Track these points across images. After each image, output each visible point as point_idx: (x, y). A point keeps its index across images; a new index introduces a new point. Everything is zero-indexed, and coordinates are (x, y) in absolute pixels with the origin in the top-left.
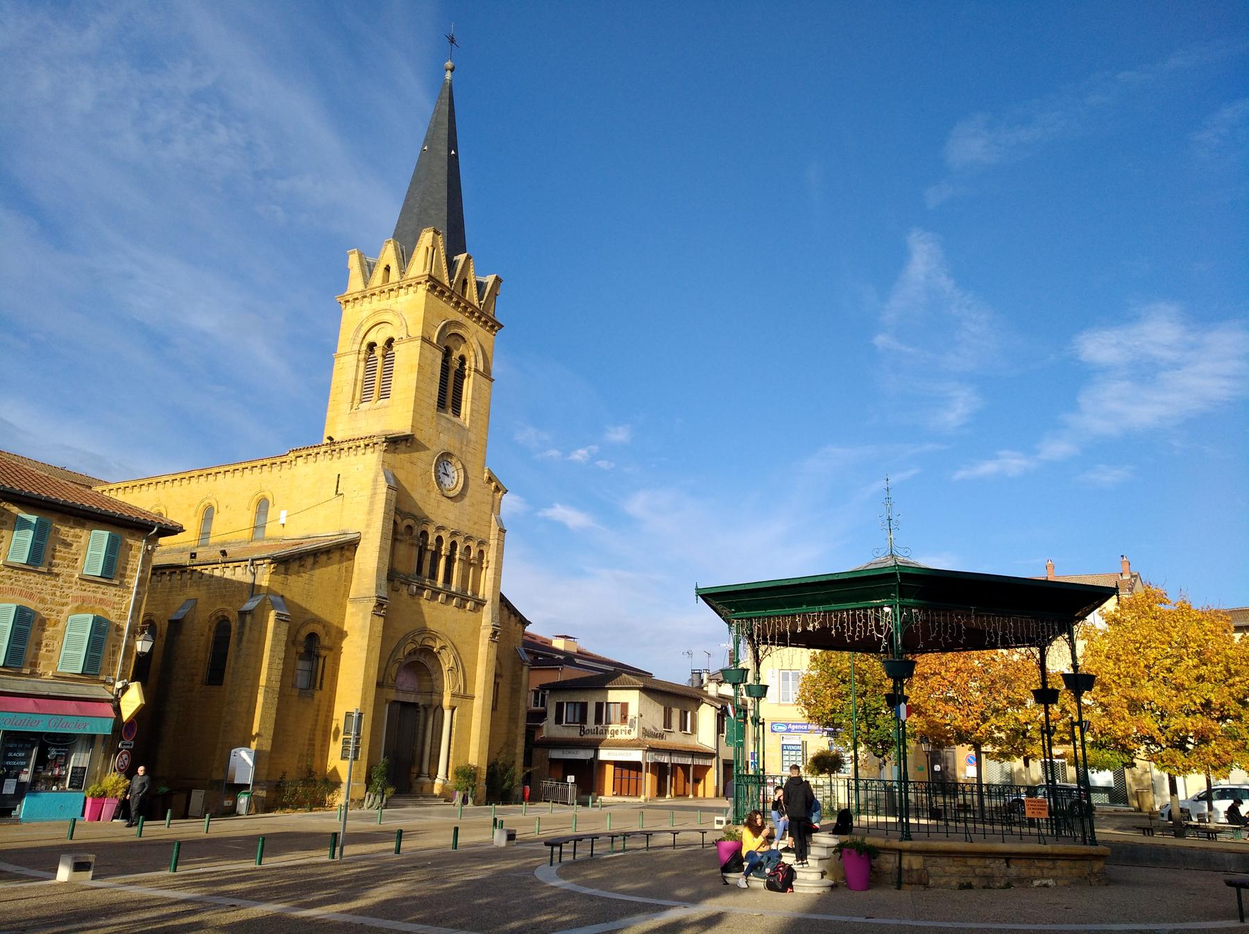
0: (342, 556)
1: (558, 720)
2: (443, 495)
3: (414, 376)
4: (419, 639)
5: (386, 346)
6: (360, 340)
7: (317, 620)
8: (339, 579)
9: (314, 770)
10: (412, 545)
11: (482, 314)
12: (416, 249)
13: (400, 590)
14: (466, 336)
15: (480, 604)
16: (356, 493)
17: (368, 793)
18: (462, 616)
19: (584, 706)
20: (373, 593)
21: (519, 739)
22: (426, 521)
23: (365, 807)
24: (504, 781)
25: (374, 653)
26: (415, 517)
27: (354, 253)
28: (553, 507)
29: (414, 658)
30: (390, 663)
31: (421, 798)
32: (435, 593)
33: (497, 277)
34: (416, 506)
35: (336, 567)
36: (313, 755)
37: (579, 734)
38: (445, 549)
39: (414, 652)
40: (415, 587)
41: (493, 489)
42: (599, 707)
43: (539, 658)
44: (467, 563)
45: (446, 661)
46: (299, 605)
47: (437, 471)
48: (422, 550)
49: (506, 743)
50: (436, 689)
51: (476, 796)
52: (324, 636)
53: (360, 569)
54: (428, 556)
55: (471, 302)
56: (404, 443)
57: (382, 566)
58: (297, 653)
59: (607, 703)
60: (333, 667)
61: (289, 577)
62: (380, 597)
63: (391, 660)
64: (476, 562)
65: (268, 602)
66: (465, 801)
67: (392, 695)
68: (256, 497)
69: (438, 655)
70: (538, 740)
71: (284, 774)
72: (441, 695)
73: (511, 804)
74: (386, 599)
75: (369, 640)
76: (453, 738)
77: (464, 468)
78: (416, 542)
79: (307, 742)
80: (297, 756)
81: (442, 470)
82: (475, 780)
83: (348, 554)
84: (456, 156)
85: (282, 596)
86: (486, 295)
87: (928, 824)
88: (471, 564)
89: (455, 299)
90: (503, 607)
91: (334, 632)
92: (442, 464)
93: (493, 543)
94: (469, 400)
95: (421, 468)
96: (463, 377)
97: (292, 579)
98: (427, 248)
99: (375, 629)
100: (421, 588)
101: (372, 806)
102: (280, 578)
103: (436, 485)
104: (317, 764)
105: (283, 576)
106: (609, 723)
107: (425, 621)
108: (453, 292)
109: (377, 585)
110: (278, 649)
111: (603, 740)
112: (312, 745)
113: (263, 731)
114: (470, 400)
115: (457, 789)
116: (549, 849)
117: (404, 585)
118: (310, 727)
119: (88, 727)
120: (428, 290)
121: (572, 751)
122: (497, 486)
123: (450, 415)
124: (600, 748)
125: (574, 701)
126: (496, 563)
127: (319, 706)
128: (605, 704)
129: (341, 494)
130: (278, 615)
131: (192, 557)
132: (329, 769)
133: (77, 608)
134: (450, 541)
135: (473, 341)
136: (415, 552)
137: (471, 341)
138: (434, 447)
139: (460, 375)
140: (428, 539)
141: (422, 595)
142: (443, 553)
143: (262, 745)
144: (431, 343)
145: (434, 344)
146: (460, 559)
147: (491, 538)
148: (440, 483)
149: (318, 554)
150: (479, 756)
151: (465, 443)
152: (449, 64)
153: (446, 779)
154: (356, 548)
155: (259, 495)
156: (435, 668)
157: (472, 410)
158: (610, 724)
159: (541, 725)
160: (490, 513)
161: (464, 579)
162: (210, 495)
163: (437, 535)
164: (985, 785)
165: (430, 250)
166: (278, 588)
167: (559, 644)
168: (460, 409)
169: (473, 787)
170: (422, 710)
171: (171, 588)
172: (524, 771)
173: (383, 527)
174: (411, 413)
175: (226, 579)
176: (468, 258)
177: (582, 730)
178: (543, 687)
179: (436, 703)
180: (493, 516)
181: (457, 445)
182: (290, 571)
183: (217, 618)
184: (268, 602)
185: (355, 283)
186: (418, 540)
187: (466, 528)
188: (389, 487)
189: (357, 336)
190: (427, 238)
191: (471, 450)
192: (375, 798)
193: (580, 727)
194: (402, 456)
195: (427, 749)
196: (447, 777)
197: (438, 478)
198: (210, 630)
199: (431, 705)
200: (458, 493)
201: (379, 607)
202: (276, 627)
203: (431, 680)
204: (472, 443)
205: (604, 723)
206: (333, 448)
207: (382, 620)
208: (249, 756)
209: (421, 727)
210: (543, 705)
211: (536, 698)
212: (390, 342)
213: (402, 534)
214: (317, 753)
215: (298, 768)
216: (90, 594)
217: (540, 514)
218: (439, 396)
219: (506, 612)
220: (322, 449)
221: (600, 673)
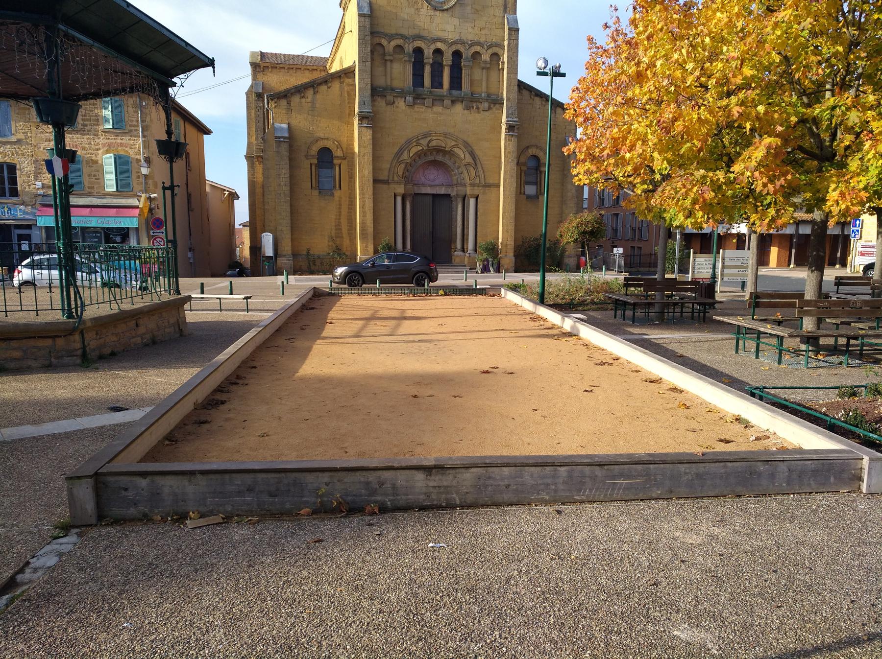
10: (405, 61)
13: (396, 103)
25: (366, 158)
36: (342, 237)
38: (447, 59)
71: (308, 250)
87: (175, 274)
116: (245, 300)
118: (334, 217)
119: (122, 223)
133: (107, 150)
136: (409, 69)
215: (329, 245)
216: (113, 141)
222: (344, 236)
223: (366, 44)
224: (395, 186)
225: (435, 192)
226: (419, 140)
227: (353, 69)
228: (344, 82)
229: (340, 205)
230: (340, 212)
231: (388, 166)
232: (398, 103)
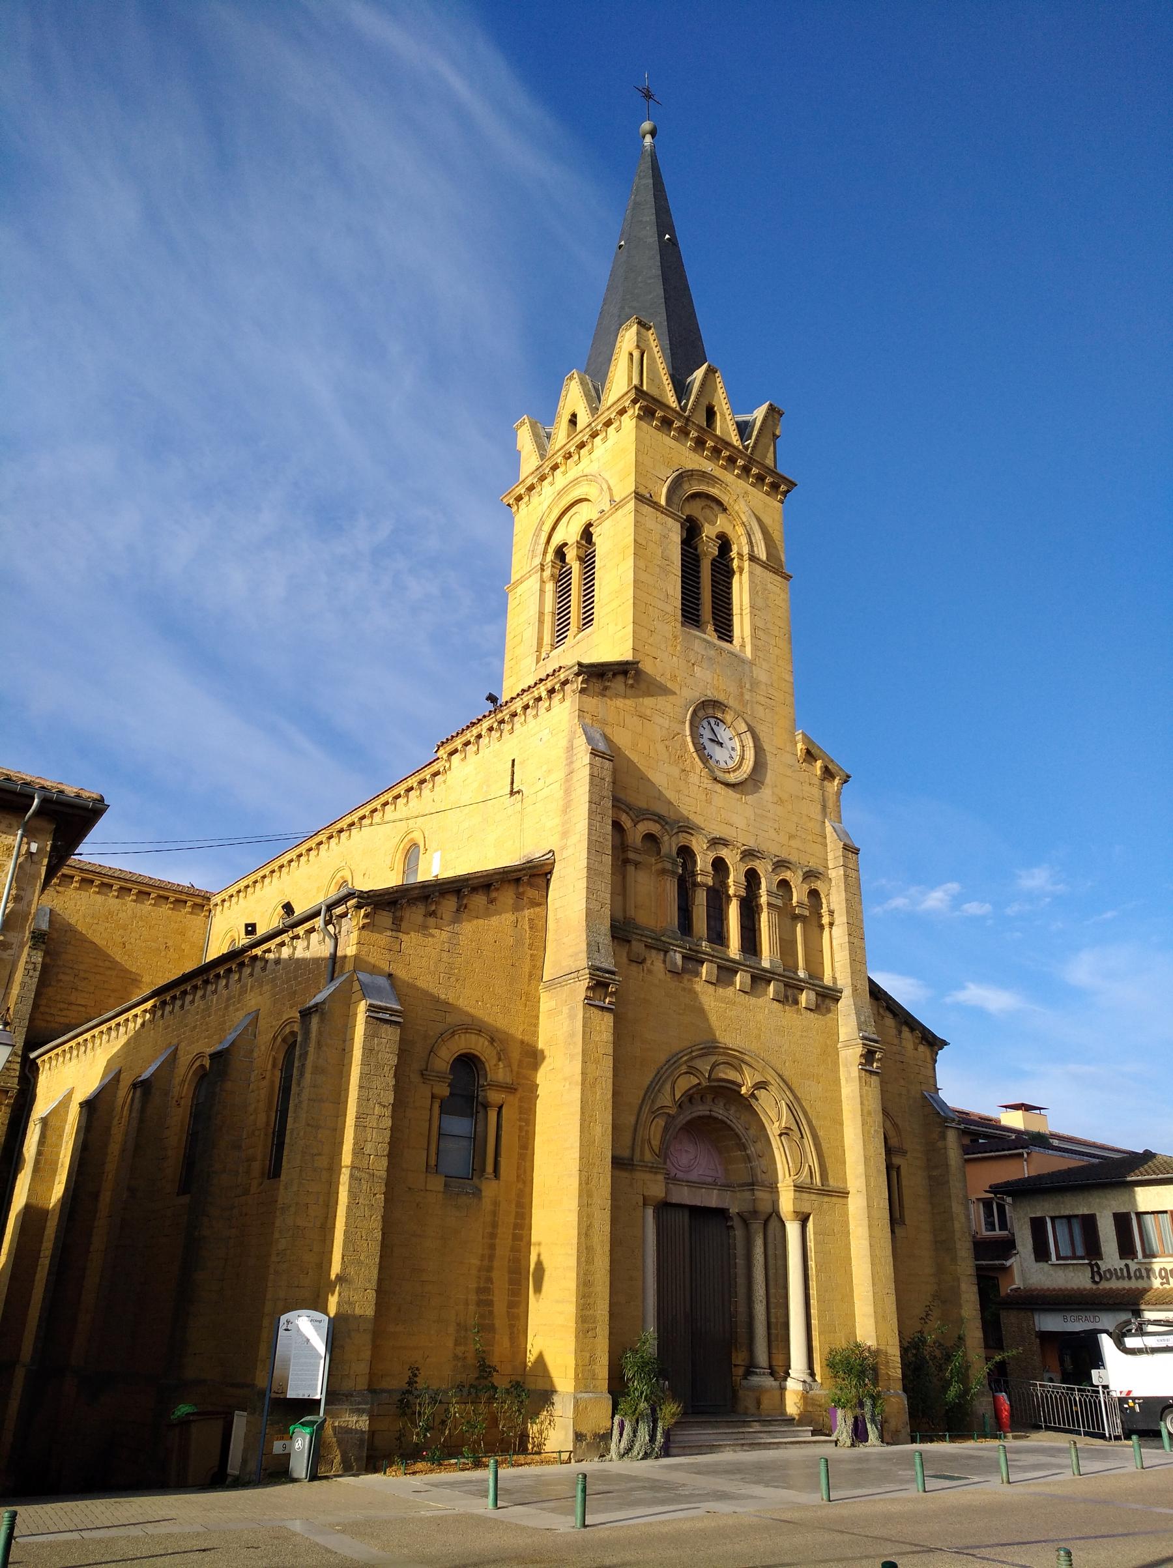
0: (519, 896)
1: (1041, 1253)
2: (715, 779)
3: (630, 562)
4: (704, 1066)
5: (583, 542)
6: (541, 547)
7: (474, 1027)
8: (519, 942)
9: (495, 1361)
10: (663, 872)
11: (751, 460)
12: (613, 363)
13: (649, 962)
14: (725, 499)
15: (828, 997)
16: (542, 781)
17: (617, 1418)
18: (788, 1017)
19: (1089, 1224)
20: (582, 962)
21: (964, 1286)
22: (687, 827)
23: (613, 1453)
24: (946, 1385)
26: (659, 819)
27: (523, 423)
28: (964, 988)
29: (701, 1110)
30: (643, 1117)
31: (757, 1427)
32: (727, 971)
33: (771, 405)
34: (660, 796)
35: (508, 918)
36: (491, 1328)
37: (1089, 1281)
38: (735, 883)
39: (691, 1097)
40: (678, 957)
41: (819, 773)
42: (1122, 1222)
43: (981, 1141)
44: (787, 915)
45: (773, 1114)
46: (431, 995)
47: (696, 736)
48: (686, 885)
49: (936, 1296)
50: (760, 1177)
51: (884, 1422)
52: (493, 1062)
53: (557, 920)
54: (701, 897)
55: (728, 439)
56: (620, 678)
57: (596, 906)
58: (433, 1097)
59: (1139, 1215)
60: (521, 1129)
61: (404, 937)
62: (599, 969)
63: (646, 1109)
64: (807, 913)
65: (356, 986)
66: (859, 1434)
67: (656, 1188)
68: (401, 847)
69: (753, 1101)
70: (1008, 1295)
71: (414, 1372)
72: (773, 1189)
73: (970, 1437)
74: (613, 973)
75: (584, 1062)
76: (813, 1284)
77: (751, 729)
78: (669, 866)
79: (473, 1297)
80: (452, 1329)
81: (707, 734)
82: (875, 1381)
83: (531, 893)
84: (673, 241)
85: (390, 975)
86: (755, 433)
88: (796, 918)
89: (693, 434)
90: (881, 1011)
91: (515, 1054)
92: (705, 723)
93: (836, 874)
94: (747, 611)
95: (661, 727)
96: (730, 573)
97: (410, 940)
98: (631, 354)
99: (596, 1038)
100: (694, 959)
101: (629, 1450)
102: (383, 938)
103: (697, 759)
104: (502, 1345)
105: (389, 933)
106: (1150, 1254)
107: (710, 1029)
108: (688, 419)
109: (588, 945)
110: (377, 1083)
111: (1145, 1291)
112: (485, 1304)
113: (352, 1271)
114: (748, 610)
115: (838, 1403)
117: (654, 952)
118: (476, 1262)
120: (639, 417)
121: (1083, 1315)
122: (826, 767)
123: (710, 635)
124: (1143, 1307)
125: (1067, 1213)
126: (848, 912)
127: (494, 1213)
128: (1133, 1217)
129: (518, 792)
130: (371, 1008)
131: (248, 933)
132: (531, 1358)
134: (743, 868)
135: (740, 508)
136: (671, 888)
137: (737, 508)
138: (684, 689)
139: (723, 571)
140: (695, 862)
141: (697, 974)
142: (731, 892)
143: (350, 1303)
144: (655, 505)
145: (660, 506)
146: (769, 904)
147: (830, 866)
148: (705, 758)
149: (466, 891)
150: (876, 1323)
151: (748, 686)
152: (647, 126)
153: (809, 1379)
154: (548, 881)
155: (406, 840)
156: (752, 1132)
157: (754, 628)
158: (1154, 1256)
160: (819, 818)
161: (786, 947)
162: (343, 864)
163: (711, 856)
165: (636, 354)
166: (377, 958)
167: (1014, 1120)
168: (731, 631)
169: (874, 1398)
170: (737, 1223)
171: (228, 999)
172: (988, 1359)
173: (590, 829)
174: (630, 628)
175: (298, 959)
176: (711, 371)
177: (1096, 1272)
178: (995, 1189)
179: (765, 1207)
180: (827, 823)
181: (733, 689)
182: (404, 925)
183: (284, 1040)
184: (356, 986)
185: (529, 461)
186: (674, 863)
187: (773, 844)
188: (595, 753)
189: (536, 543)
190: (628, 338)
191: (763, 700)
192: (635, 1431)
193: (1090, 1264)
194: (620, 703)
195: (760, 1309)
196: (812, 1374)
197: (700, 749)
198: (274, 1066)
199: (755, 1213)
200: (745, 776)
201: (600, 992)
202: (369, 1036)
203: (748, 1159)
204: (763, 687)
205: (1140, 1254)
206: (499, 716)
207: (609, 1019)
208: (317, 1329)
209: (740, 1261)
210: (1004, 1226)
211: (989, 1214)
212: (587, 535)
213: (636, 851)
214: (500, 1322)
215: (456, 1357)
217: (949, 1000)
218: (682, 598)
219: (889, 1021)
220: (484, 725)
221: (1098, 1160)
222: (498, 1323)
223: (603, 815)
224: (647, 1176)
225: (697, 1202)
227: (547, 869)
228: (523, 894)
229: (494, 1225)
230: (492, 1247)
231: (632, 1120)
232: (652, 964)
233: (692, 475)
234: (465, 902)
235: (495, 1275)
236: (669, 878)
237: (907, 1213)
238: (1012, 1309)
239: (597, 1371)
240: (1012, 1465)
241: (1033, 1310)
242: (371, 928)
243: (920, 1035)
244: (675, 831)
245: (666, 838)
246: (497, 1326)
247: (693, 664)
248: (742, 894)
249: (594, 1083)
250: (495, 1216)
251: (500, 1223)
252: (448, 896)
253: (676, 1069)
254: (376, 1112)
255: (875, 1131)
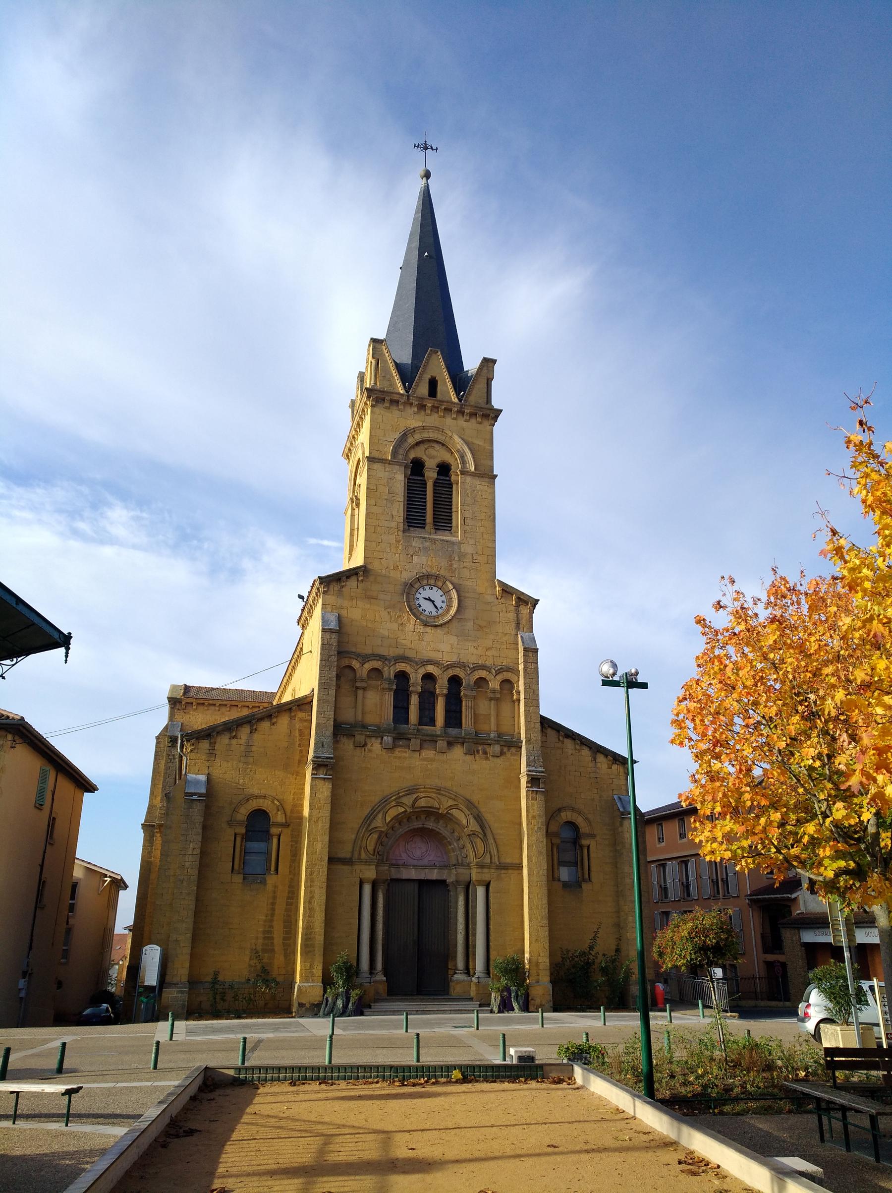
13: (369, 745)
56: (354, 578)
71: (216, 974)
78: (386, 686)
79: (261, 935)
127: (274, 892)
151: (456, 558)
159: (793, 896)
160: (514, 632)
164: (649, 981)
181: (444, 563)
195: (460, 938)
215: (250, 966)
224: (363, 867)
225: (422, 877)
226: (400, 797)
227: (309, 700)
228: (295, 716)
229: (275, 898)
230: (273, 910)
233: (414, 431)
234: (255, 727)
235: (275, 924)
236: (387, 693)
237: (593, 874)
238: (788, 927)
239: (315, 972)
240: (548, 1019)
241: (799, 929)
242: (196, 751)
243: (612, 759)
244: (392, 664)
245: (386, 669)
246: (276, 950)
247: (412, 556)
248: (444, 692)
249: (317, 821)
250: (275, 893)
251: (278, 897)
252: (245, 726)
253: (387, 804)
254: (191, 846)
255: (538, 828)
